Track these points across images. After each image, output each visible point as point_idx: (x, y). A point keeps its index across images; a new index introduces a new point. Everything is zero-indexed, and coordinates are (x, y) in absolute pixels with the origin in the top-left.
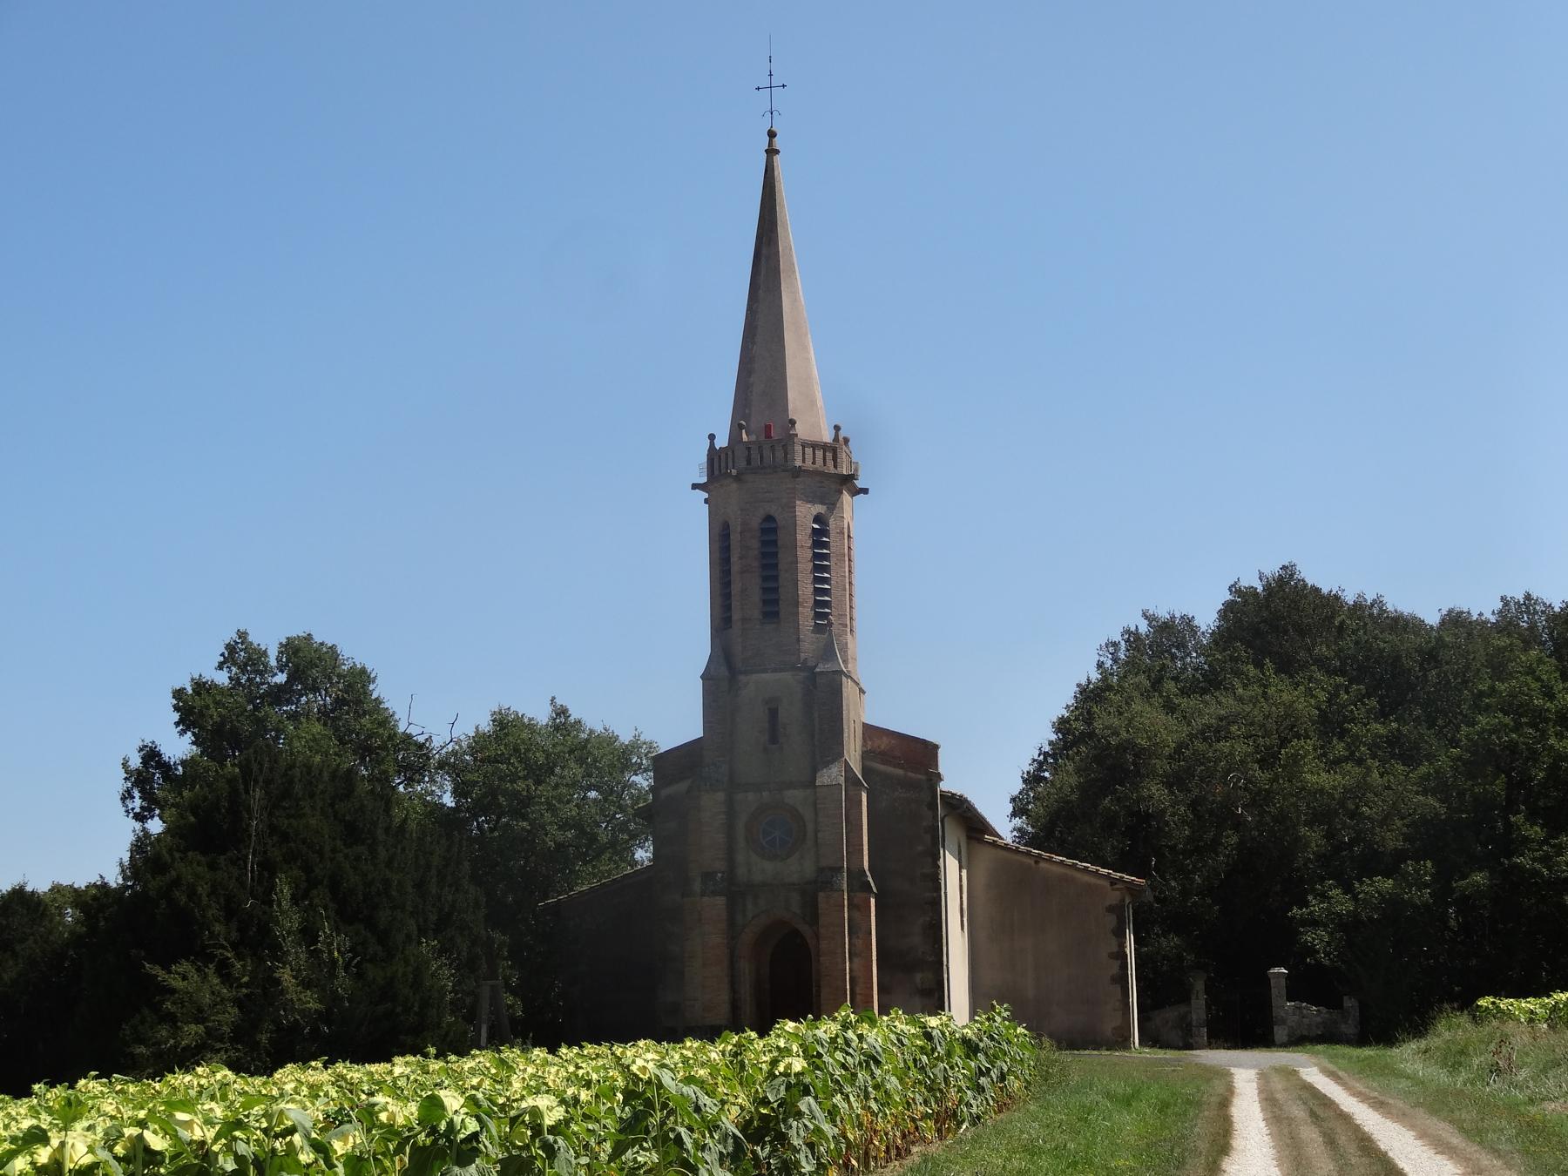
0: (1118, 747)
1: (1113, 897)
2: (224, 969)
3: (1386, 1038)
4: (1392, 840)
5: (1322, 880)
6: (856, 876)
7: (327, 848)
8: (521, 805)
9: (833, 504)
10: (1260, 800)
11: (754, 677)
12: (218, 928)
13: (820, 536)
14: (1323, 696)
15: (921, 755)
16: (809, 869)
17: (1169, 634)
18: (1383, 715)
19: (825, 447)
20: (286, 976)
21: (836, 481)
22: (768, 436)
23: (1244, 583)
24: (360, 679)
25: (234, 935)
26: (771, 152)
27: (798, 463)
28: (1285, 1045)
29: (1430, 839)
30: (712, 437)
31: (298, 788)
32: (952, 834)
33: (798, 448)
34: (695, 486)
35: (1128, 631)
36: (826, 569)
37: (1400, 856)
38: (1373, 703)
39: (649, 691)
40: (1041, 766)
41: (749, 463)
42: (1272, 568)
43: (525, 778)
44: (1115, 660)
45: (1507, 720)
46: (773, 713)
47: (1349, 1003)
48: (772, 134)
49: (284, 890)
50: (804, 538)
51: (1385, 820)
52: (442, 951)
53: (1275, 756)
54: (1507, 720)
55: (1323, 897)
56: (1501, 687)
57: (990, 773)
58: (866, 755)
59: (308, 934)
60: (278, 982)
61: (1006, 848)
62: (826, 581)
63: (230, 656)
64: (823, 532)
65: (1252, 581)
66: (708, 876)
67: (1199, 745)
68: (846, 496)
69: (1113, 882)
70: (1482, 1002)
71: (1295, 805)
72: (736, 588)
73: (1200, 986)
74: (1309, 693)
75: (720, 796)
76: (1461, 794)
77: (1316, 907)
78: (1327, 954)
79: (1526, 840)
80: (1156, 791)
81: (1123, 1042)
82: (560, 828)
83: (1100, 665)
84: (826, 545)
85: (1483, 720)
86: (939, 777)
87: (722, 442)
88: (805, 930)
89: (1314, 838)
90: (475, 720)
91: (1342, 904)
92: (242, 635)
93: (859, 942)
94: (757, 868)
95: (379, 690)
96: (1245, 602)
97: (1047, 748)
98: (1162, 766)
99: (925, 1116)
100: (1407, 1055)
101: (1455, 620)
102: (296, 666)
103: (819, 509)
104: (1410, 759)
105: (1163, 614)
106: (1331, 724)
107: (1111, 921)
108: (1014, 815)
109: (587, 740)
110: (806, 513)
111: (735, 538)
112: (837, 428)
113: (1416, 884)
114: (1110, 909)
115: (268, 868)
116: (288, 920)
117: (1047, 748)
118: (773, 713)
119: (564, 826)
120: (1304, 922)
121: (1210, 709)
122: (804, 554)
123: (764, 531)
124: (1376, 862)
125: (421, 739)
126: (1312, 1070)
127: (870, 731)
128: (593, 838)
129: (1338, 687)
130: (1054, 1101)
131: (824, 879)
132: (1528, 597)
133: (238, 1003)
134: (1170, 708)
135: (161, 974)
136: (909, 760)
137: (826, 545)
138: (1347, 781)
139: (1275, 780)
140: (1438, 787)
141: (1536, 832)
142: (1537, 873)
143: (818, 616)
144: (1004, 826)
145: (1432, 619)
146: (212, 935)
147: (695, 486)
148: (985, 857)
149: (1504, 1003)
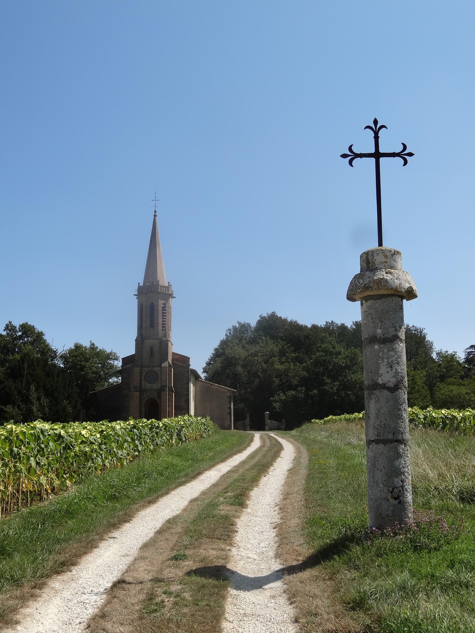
0: (231, 358)
1: (229, 394)
2: (19, 407)
3: (291, 429)
4: (295, 382)
5: (278, 391)
6: (170, 388)
7: (43, 378)
8: (82, 368)
9: (167, 300)
10: (264, 371)
11: (148, 341)
12: (17, 397)
13: (164, 309)
14: (281, 346)
15: (185, 360)
16: (159, 386)
17: (244, 327)
18: (295, 351)
19: (166, 287)
20: (35, 409)
21: (168, 295)
22: (153, 284)
23: (263, 315)
24: (40, 335)
25: (20, 399)
26: (155, 216)
27: (160, 291)
28: (267, 431)
29: (304, 382)
30: (139, 283)
31: (35, 363)
32: (192, 379)
33: (160, 287)
34: (134, 295)
35: (233, 326)
36: (165, 316)
37: (297, 386)
38: (293, 348)
39: (119, 342)
40: (211, 360)
41: (148, 290)
42: (270, 312)
43: (84, 361)
44: (230, 334)
45: (323, 354)
46: (152, 349)
47: (283, 421)
48: (155, 212)
49: (33, 388)
50: (160, 308)
51: (294, 377)
52: (69, 404)
53: (268, 360)
54: (323, 354)
55: (279, 395)
56: (323, 346)
57: (198, 364)
58: (172, 360)
59: (39, 399)
60: (32, 410)
61: (204, 382)
62: (165, 319)
63: (7, 328)
64: (165, 307)
65: (265, 315)
66: (135, 387)
67: (250, 358)
68: (170, 299)
69: (229, 391)
70: (312, 421)
71: (272, 373)
72: (144, 320)
73: (248, 416)
74: (277, 346)
75: (139, 369)
76: (313, 371)
77: (277, 397)
78: (279, 409)
79: (327, 383)
80: (240, 369)
81: (229, 428)
82: (92, 373)
83: (226, 335)
84: (165, 310)
85: (318, 354)
86: (190, 365)
87: (141, 284)
88: (158, 400)
89: (277, 381)
90: (71, 345)
91: (283, 397)
92: (10, 322)
93: (170, 403)
94: (148, 386)
95: (45, 337)
96: (263, 321)
97: (212, 356)
98: (241, 362)
99: (198, 435)
100: (294, 432)
101: (314, 327)
102: (25, 331)
103: (164, 302)
104: (301, 362)
105: (242, 322)
106: (282, 353)
107: (228, 400)
108: (203, 372)
109: (99, 352)
110: (161, 302)
111: (144, 307)
112: (169, 283)
113: (301, 393)
114: (228, 397)
115: (28, 383)
116: (34, 395)
117: (212, 356)
118: (152, 349)
119: (93, 373)
120: (274, 401)
121: (253, 349)
122: (160, 312)
123: (151, 306)
124: (291, 387)
125: (55, 350)
126: (272, 434)
127: (174, 354)
128: (100, 376)
129: (284, 344)
130: (28, 619)
131: (162, 389)
132: (332, 321)
133: (22, 415)
134: (243, 347)
135: (4, 408)
136: (182, 361)
137: (165, 310)
138: (286, 367)
139: (268, 366)
140: (307, 369)
141: (329, 381)
142: (329, 391)
143: (163, 327)
144: (203, 376)
145: (309, 326)
146: (15, 398)
147: (134, 295)
148: (199, 384)
149: (317, 421)
